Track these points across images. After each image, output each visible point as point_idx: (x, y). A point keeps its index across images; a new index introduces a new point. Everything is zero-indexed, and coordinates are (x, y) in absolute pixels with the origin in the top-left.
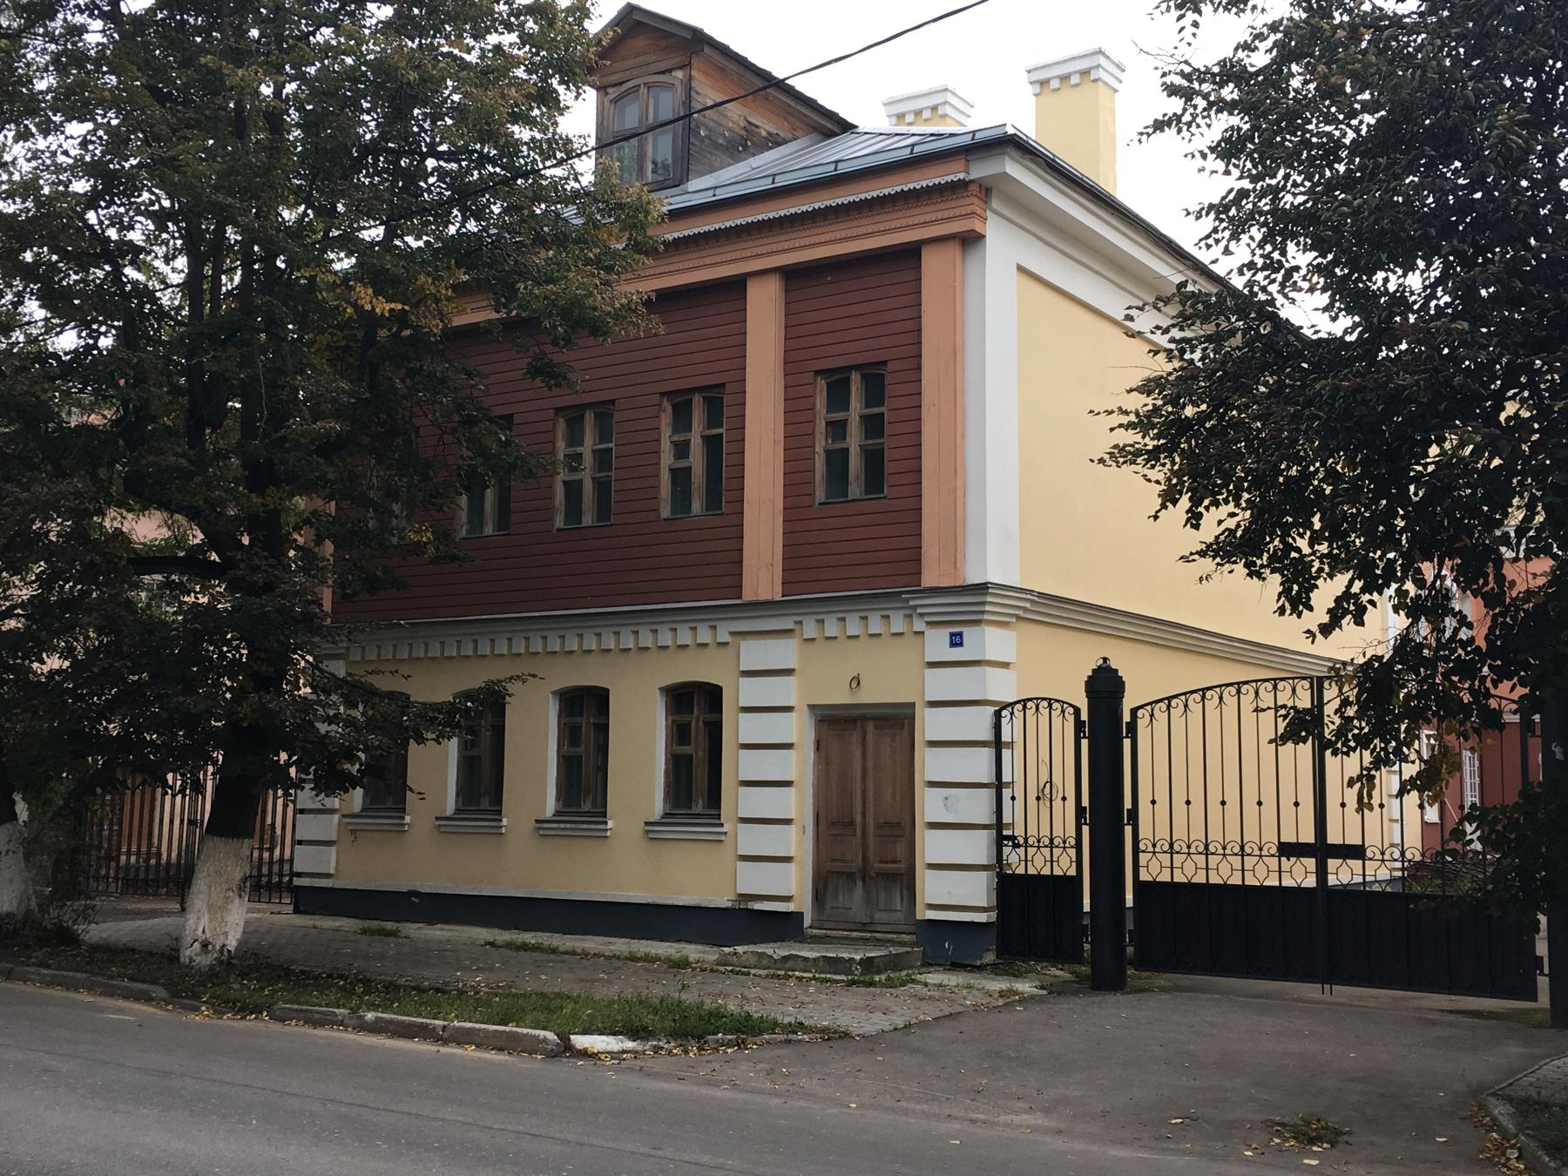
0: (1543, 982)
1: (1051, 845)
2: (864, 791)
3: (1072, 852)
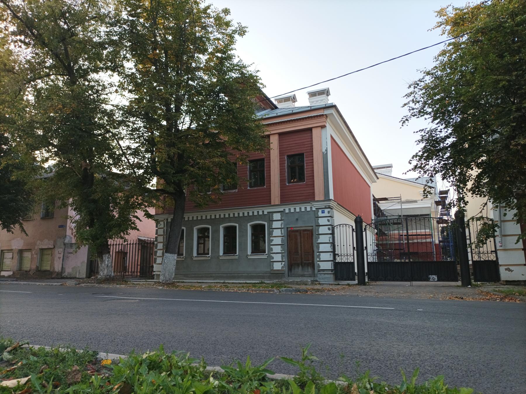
0: (356, 277)
1: (347, 255)
2: (301, 246)
3: (352, 257)
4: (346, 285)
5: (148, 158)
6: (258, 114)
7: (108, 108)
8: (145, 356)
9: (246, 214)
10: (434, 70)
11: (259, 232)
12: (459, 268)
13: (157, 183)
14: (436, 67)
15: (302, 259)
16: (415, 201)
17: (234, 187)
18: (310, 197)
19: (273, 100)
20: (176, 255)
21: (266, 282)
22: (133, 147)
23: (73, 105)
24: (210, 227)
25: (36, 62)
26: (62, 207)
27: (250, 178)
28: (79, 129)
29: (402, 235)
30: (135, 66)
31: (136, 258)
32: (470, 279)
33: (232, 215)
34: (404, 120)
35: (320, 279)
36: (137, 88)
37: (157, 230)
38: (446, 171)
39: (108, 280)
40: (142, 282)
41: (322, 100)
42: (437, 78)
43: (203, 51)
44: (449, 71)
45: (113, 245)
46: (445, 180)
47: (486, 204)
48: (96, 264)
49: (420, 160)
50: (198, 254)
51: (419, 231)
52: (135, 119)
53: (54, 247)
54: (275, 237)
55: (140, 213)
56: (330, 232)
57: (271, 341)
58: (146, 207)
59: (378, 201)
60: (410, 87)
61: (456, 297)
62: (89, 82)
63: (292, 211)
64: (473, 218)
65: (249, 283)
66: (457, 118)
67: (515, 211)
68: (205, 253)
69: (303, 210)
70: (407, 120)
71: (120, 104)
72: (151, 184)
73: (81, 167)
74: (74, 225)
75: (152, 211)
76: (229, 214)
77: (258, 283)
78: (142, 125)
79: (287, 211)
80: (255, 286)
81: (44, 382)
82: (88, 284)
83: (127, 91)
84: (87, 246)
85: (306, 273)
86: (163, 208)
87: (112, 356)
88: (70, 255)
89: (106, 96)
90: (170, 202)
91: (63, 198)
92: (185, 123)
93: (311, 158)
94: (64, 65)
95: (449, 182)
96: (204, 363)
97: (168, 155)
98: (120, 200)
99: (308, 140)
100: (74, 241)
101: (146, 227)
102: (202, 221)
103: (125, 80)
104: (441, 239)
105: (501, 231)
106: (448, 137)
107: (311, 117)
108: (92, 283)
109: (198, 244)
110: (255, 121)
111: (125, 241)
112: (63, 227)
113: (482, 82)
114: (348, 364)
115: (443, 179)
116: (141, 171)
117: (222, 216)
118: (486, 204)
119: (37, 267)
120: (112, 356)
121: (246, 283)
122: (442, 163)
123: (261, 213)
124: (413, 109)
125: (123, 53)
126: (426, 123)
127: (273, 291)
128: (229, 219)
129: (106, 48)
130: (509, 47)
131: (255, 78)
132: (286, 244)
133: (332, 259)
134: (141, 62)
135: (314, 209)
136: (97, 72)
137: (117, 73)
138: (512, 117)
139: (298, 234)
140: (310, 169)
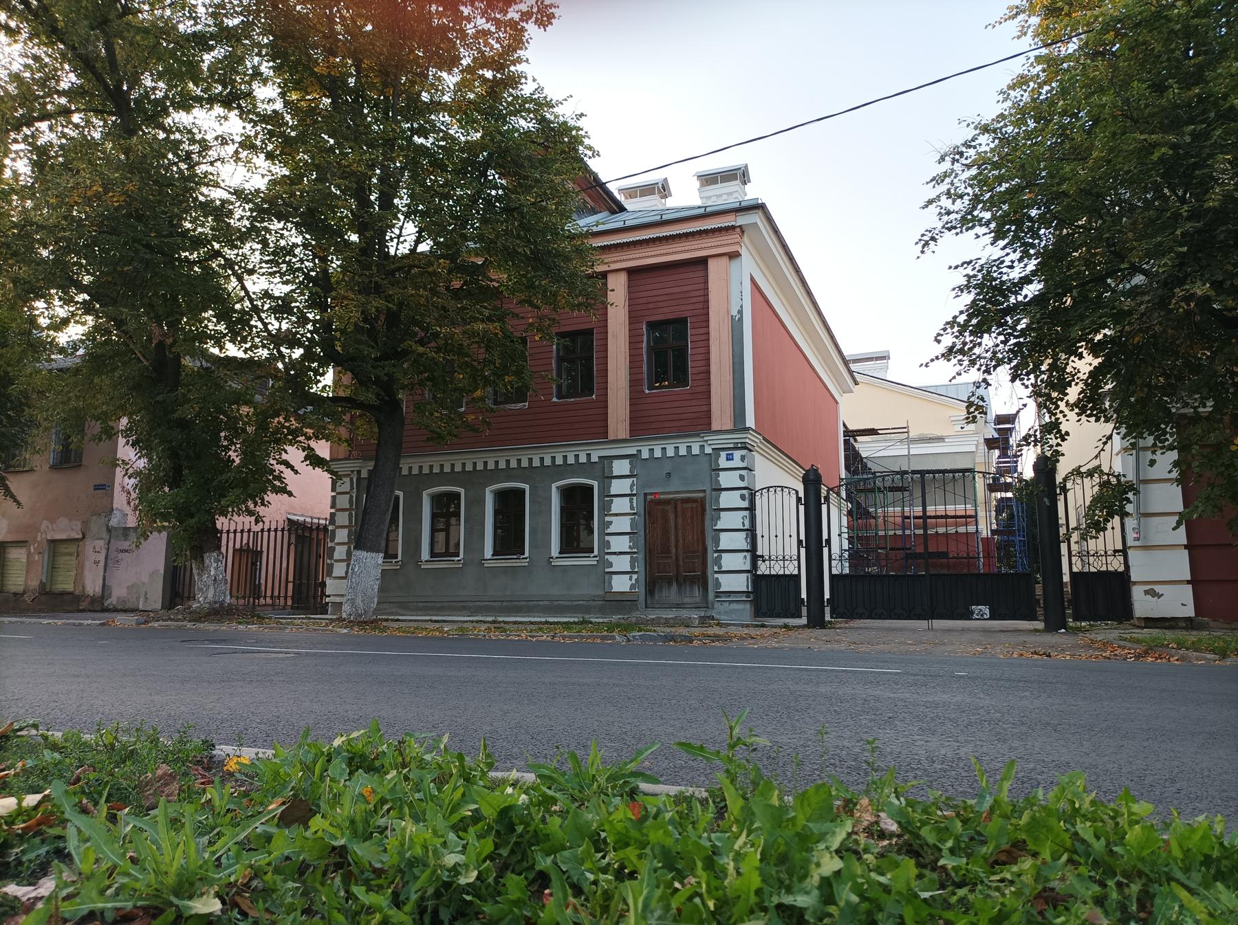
0: (804, 610)
1: (784, 559)
3: (796, 563)
4: (781, 627)
5: (315, 322)
6: (582, 222)
7: (217, 194)
8: (337, 742)
9: (548, 462)
10: (999, 122)
11: (579, 507)
12: (1039, 589)
13: (335, 382)
14: (1002, 116)
15: (678, 566)
16: (940, 439)
17: (521, 396)
18: (701, 423)
19: (613, 187)
20: (382, 555)
21: (593, 620)
22: (277, 294)
23: (130, 187)
24: (462, 491)
25: (33, 79)
26: (104, 437)
27: (559, 375)
28: (143, 246)
29: (909, 518)
30: (283, 95)
31: (284, 565)
32: (1064, 617)
33: (513, 464)
34: (926, 238)
35: (719, 613)
36: (285, 149)
37: (334, 498)
38: (1023, 360)
39: (218, 613)
40: (299, 619)
41: (730, 194)
42: (1004, 141)
43: (451, 62)
44: (1032, 124)
45: (228, 532)
46: (1018, 382)
47: (1110, 437)
48: (188, 573)
49: (961, 333)
50: (433, 554)
51: (950, 508)
52: (281, 225)
53: (84, 537)
54: (616, 515)
55: (294, 455)
56: (745, 504)
57: (626, 733)
58: (309, 438)
59: (854, 436)
60: (942, 159)
61: (1035, 653)
62: (169, 131)
63: (658, 454)
64: (1077, 472)
65: (554, 623)
66: (1046, 236)
67: (1174, 455)
68: (451, 552)
69: (683, 452)
70: (933, 239)
71: (247, 186)
72: (320, 385)
73: (150, 340)
74: (132, 481)
75: (323, 449)
76: (508, 462)
77: (575, 623)
78: (299, 240)
79: (645, 455)
80: (569, 629)
81: (85, 801)
82: (169, 623)
83: (262, 156)
84: (164, 534)
85: (687, 600)
86: (350, 442)
87: (248, 754)
88: (121, 556)
89: (210, 169)
90: (366, 429)
91: (104, 417)
92: (405, 238)
93: (704, 330)
94: (106, 86)
95: (1027, 387)
96: (488, 756)
97: (363, 312)
98: (245, 424)
99: (697, 287)
100: (132, 521)
101: (308, 489)
102: (442, 478)
103: (258, 128)
104: (994, 527)
105: (1138, 507)
106: (1026, 280)
107: (706, 232)
108: (178, 620)
109: (434, 531)
110: (572, 237)
111: (257, 522)
112: (105, 487)
113: (1111, 150)
114: (815, 777)
115: (1013, 380)
116: (298, 353)
117: (491, 466)
118: (1110, 437)
119: (43, 585)
120: (248, 754)
121: (547, 622)
122: (1013, 341)
123: (583, 459)
124: (948, 213)
125: (252, 61)
126: (978, 246)
127: (613, 638)
128: (509, 474)
129: (212, 48)
130: (1177, 68)
131: (574, 133)
132: (642, 533)
133: (748, 567)
134: (298, 85)
135: (708, 450)
136: (188, 109)
137: (236, 112)
138: (1178, 232)
139: (669, 508)
140: (700, 357)
